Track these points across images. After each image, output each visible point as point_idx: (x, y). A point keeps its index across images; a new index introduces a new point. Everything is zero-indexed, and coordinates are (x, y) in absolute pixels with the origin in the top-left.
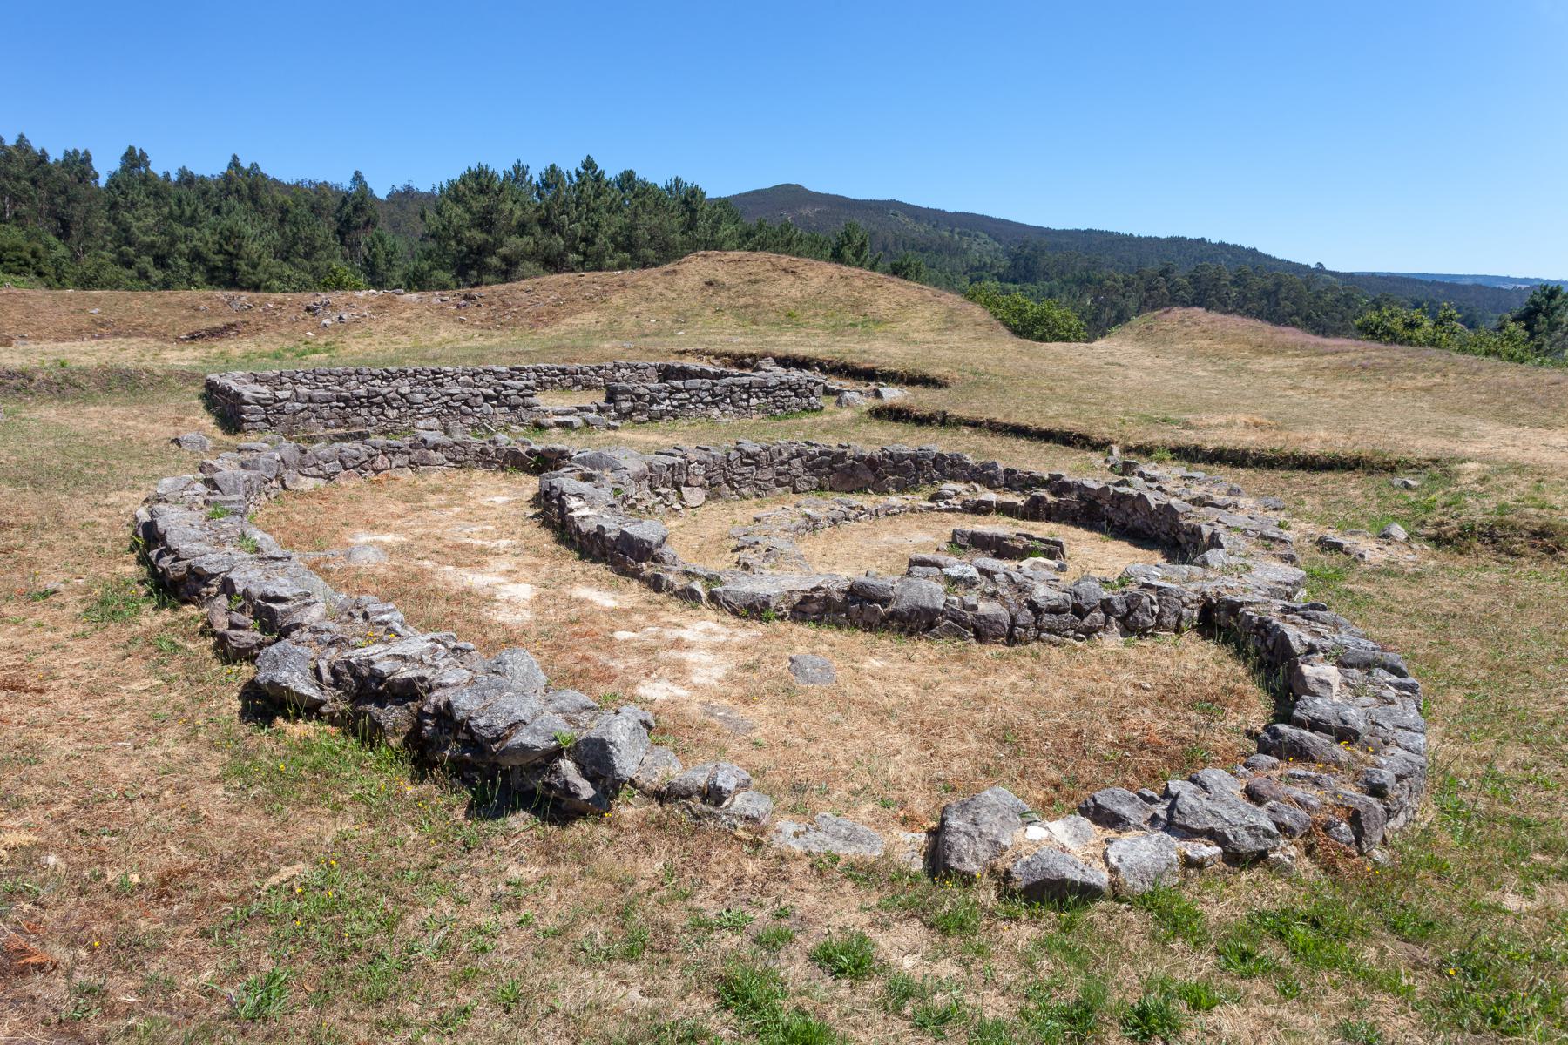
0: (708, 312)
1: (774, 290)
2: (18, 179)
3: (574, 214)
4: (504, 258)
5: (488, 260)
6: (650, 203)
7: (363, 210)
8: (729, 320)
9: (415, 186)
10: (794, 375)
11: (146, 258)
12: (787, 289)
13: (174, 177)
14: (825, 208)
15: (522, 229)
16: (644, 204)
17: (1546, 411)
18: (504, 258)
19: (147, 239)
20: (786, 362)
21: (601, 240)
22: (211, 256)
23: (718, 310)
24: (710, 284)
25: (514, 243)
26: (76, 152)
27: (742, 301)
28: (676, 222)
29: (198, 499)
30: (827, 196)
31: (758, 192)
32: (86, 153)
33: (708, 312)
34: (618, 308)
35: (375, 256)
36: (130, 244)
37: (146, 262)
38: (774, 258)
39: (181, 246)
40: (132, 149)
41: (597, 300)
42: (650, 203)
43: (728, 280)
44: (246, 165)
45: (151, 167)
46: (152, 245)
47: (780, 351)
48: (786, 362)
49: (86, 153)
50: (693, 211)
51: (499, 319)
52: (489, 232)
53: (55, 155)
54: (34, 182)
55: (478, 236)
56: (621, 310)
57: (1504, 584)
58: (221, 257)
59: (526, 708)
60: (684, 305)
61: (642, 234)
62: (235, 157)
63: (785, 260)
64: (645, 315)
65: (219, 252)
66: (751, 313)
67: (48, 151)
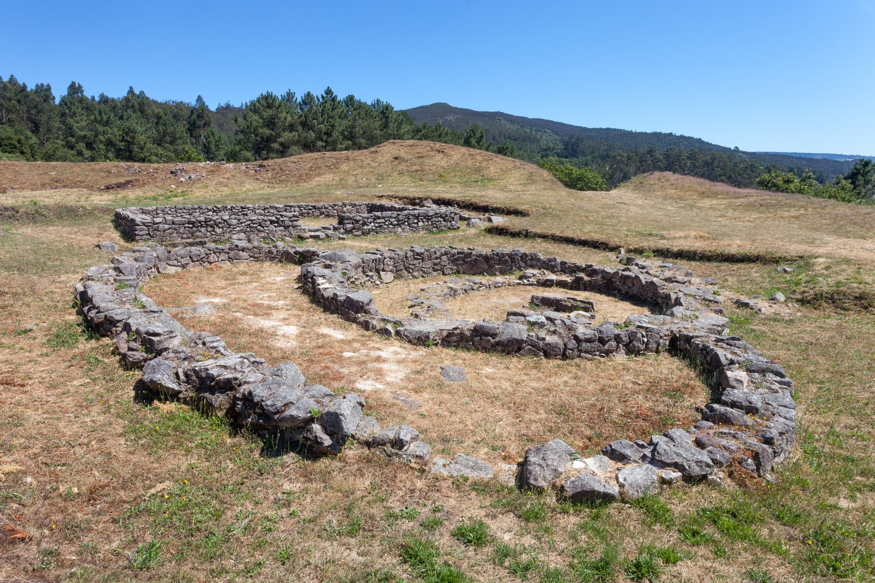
0: (395, 174)
1: (432, 162)
2: (10, 100)
3: (321, 119)
4: (281, 144)
5: (272, 145)
6: (363, 113)
7: (202, 117)
8: (407, 179)
9: (232, 104)
10: (443, 209)
11: (81, 144)
12: (439, 161)
13: (97, 99)
14: (460, 116)
15: (291, 128)
16: (359, 114)
17: (863, 229)
18: (281, 144)
19: (82, 133)
20: (439, 202)
21: (335, 134)
22: (118, 143)
23: (401, 173)
24: (396, 158)
25: (287, 136)
26: (42, 85)
27: (414, 168)
28: (378, 124)
29: (110, 278)
30: (462, 109)
31: (423, 107)
32: (48, 85)
33: (395, 174)
34: (345, 172)
35: (209, 143)
36: (73, 136)
37: (81, 146)
38: (432, 144)
39: (101, 137)
40: (73, 83)
41: (333, 167)
42: (363, 113)
43: (406, 156)
44: (137, 92)
45: (84, 93)
46: (85, 137)
47: (435, 196)
48: (439, 202)
49: (48, 85)
50: (387, 118)
51: (278, 178)
52: (273, 130)
54: (19, 101)
55: (267, 132)
56: (347, 173)
57: (839, 326)
58: (123, 143)
59: (294, 395)
60: (382, 170)
61: (358, 130)
62: (131, 88)
63: (438, 145)
64: (360, 176)
65: (122, 141)
66: (419, 175)
67: (27, 84)
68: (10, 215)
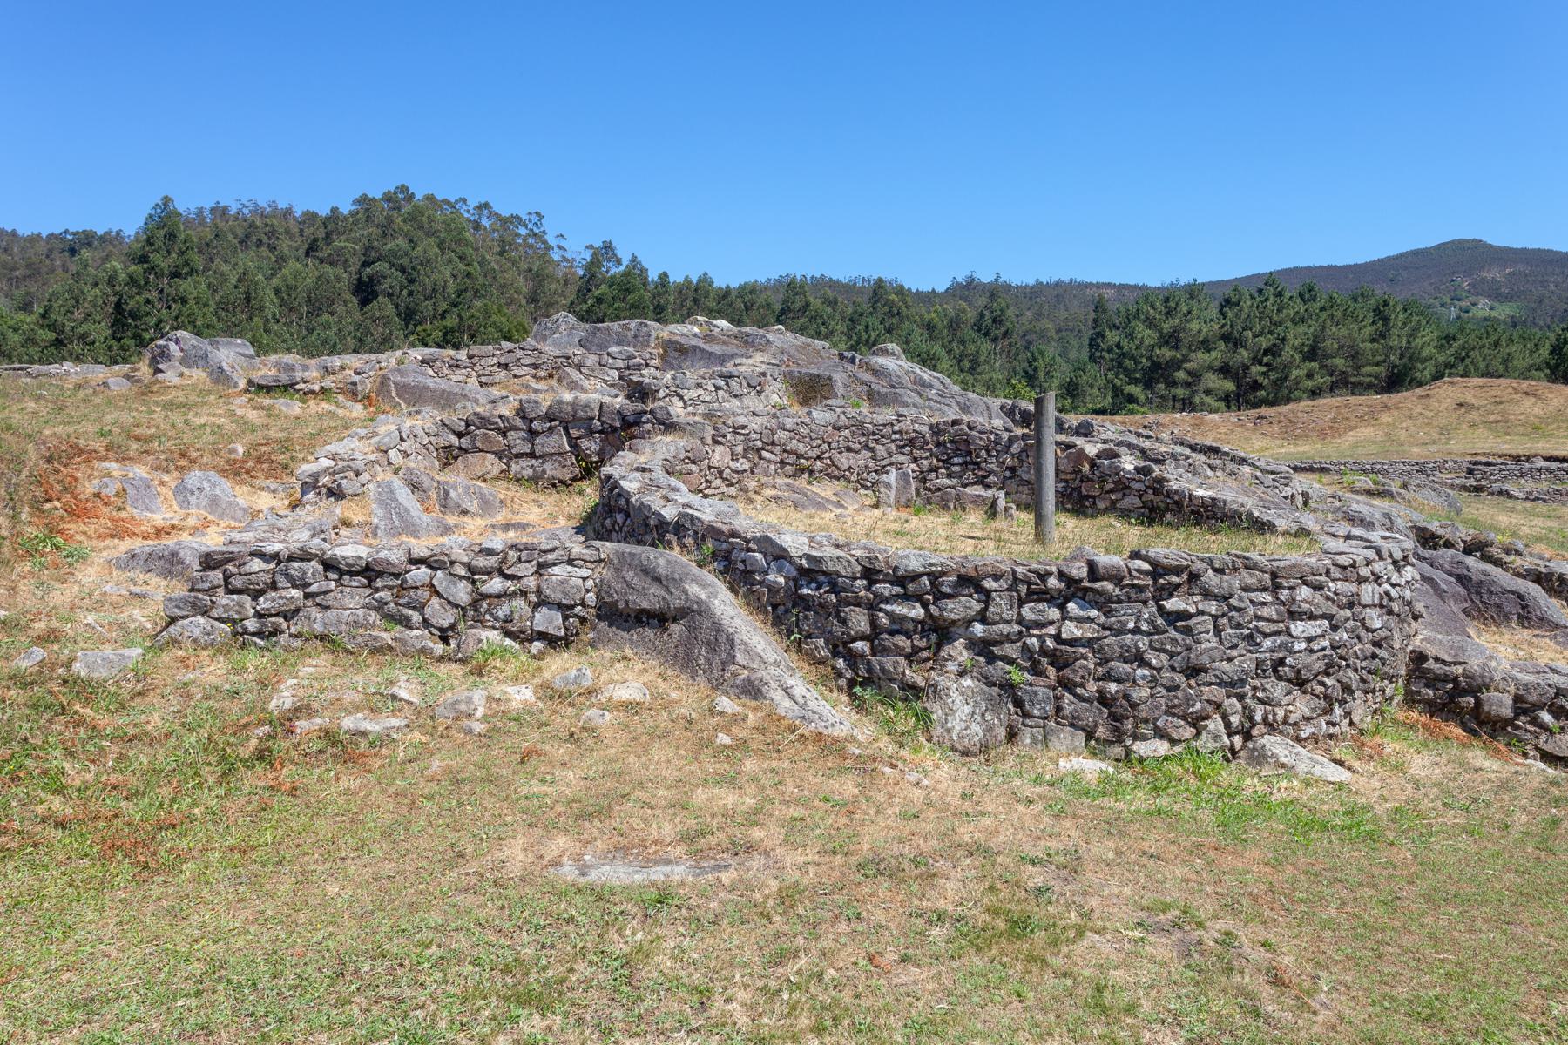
0: (1465, 426)
1: (1518, 410)
3: (1258, 328)
4: (1190, 373)
5: (1176, 374)
6: (1338, 314)
7: (1001, 322)
8: (1482, 432)
9: (977, 276)
10: (1554, 465)
12: (1530, 408)
14: (1520, 267)
15: (1206, 346)
16: (1332, 316)
18: (1190, 373)
20: (1550, 459)
21: (1288, 353)
23: (1473, 425)
24: (1461, 405)
25: (1200, 358)
27: (1492, 418)
28: (1369, 330)
29: (81, 644)
30: (1524, 251)
31: (1416, 253)
33: (1465, 426)
34: (1388, 424)
35: (1036, 369)
38: (1515, 383)
41: (1371, 416)
42: (1338, 314)
43: (1477, 403)
47: (1545, 453)
48: (1550, 459)
50: (1386, 320)
51: (1290, 431)
52: (1176, 348)
53: (346, 208)
55: (1167, 353)
56: (1392, 425)
60: (1442, 422)
61: (1330, 345)
63: (1525, 385)
64: (1413, 429)
66: (1503, 425)
68: (1567, 475)
